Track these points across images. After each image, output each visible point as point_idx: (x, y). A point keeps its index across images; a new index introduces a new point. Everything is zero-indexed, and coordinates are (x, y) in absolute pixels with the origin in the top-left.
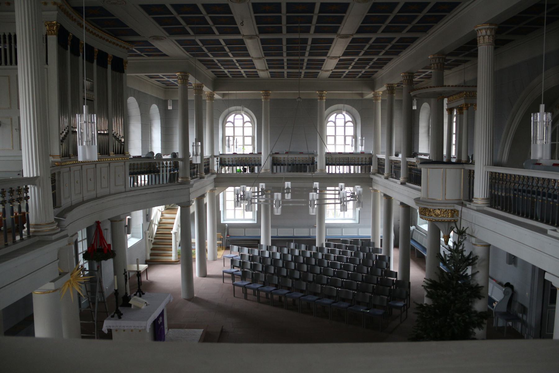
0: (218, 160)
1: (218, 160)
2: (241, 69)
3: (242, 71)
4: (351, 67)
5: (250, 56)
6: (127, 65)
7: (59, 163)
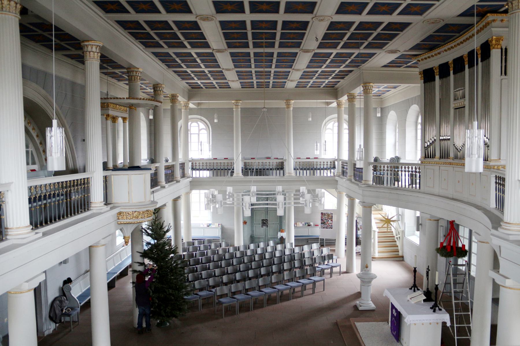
2: (213, 80)
3: (199, 82)
4: (315, 78)
5: (220, 67)
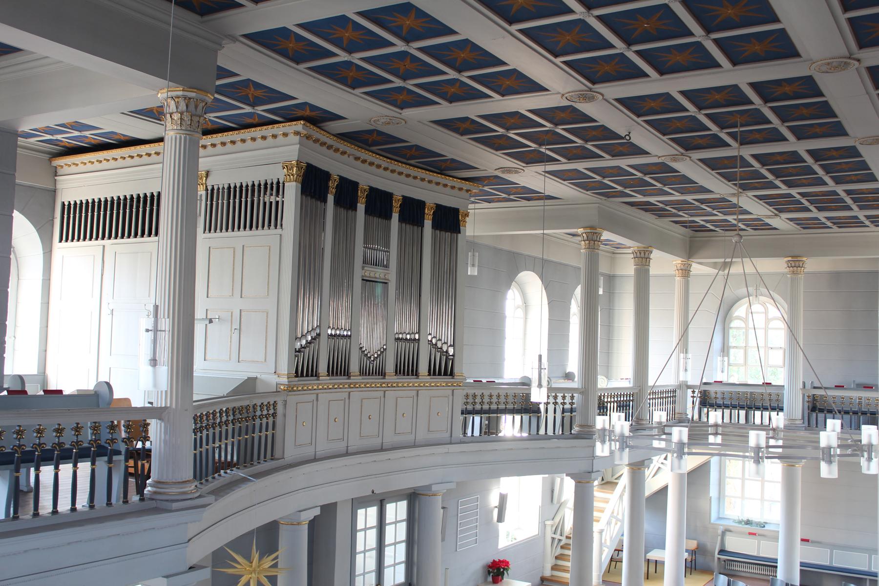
0: (695, 395)
1: (695, 395)
6: (467, 219)
7: (286, 386)
